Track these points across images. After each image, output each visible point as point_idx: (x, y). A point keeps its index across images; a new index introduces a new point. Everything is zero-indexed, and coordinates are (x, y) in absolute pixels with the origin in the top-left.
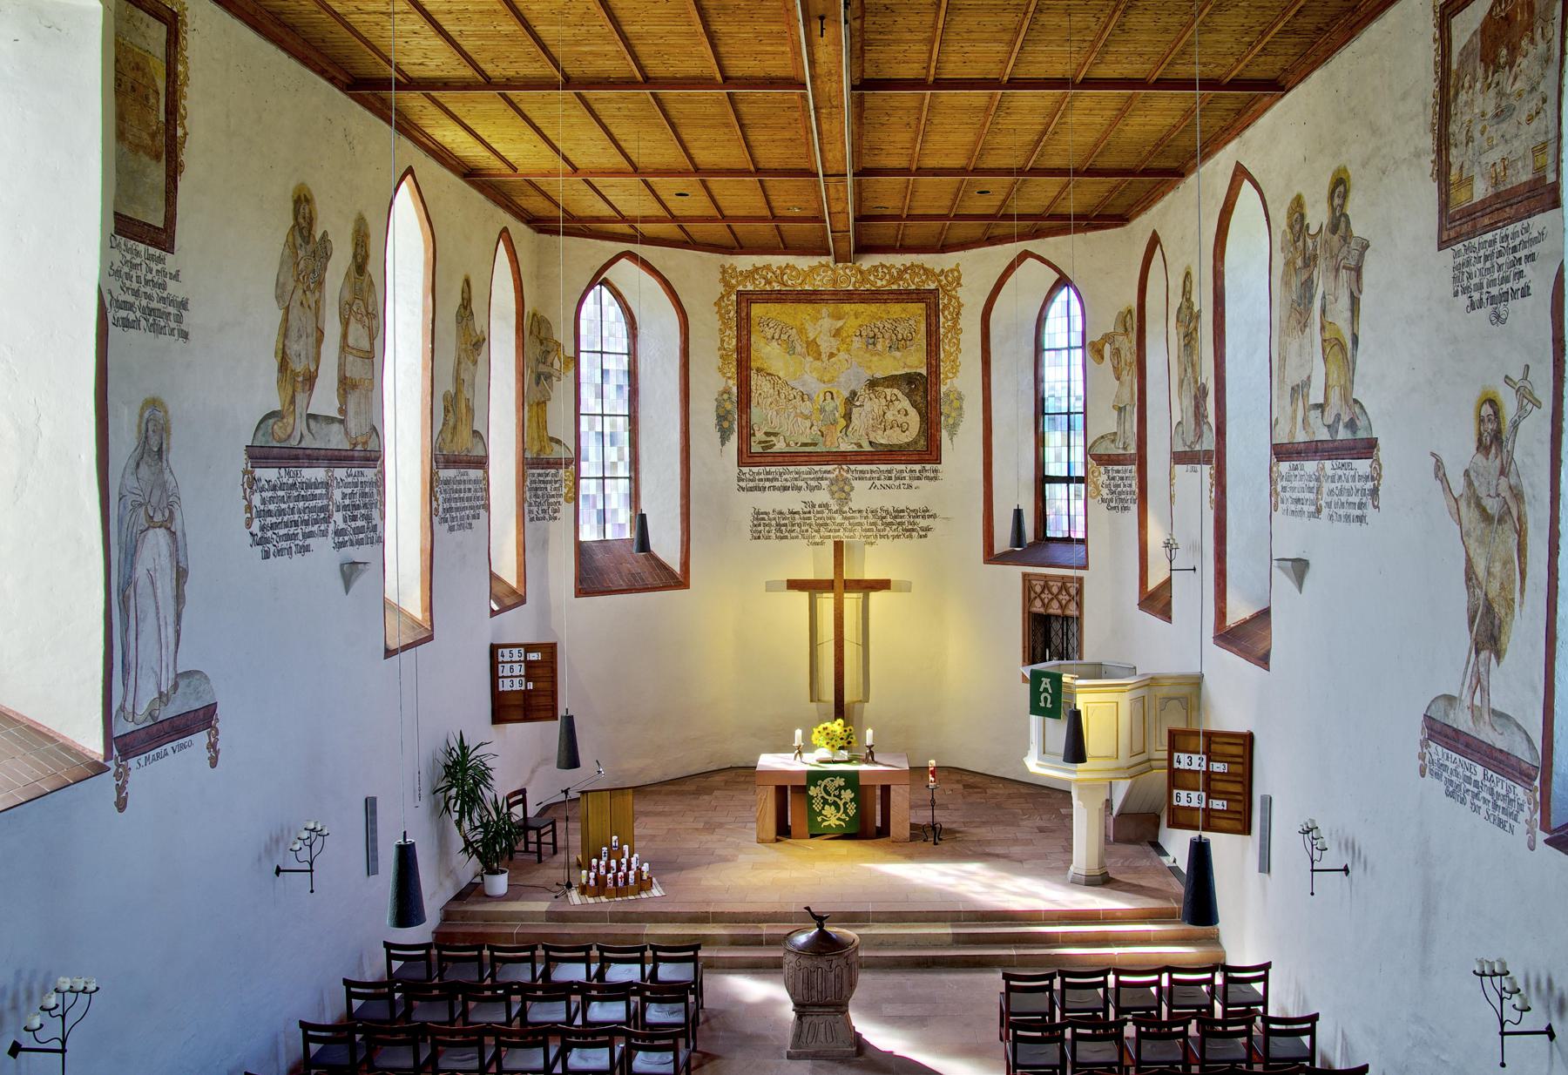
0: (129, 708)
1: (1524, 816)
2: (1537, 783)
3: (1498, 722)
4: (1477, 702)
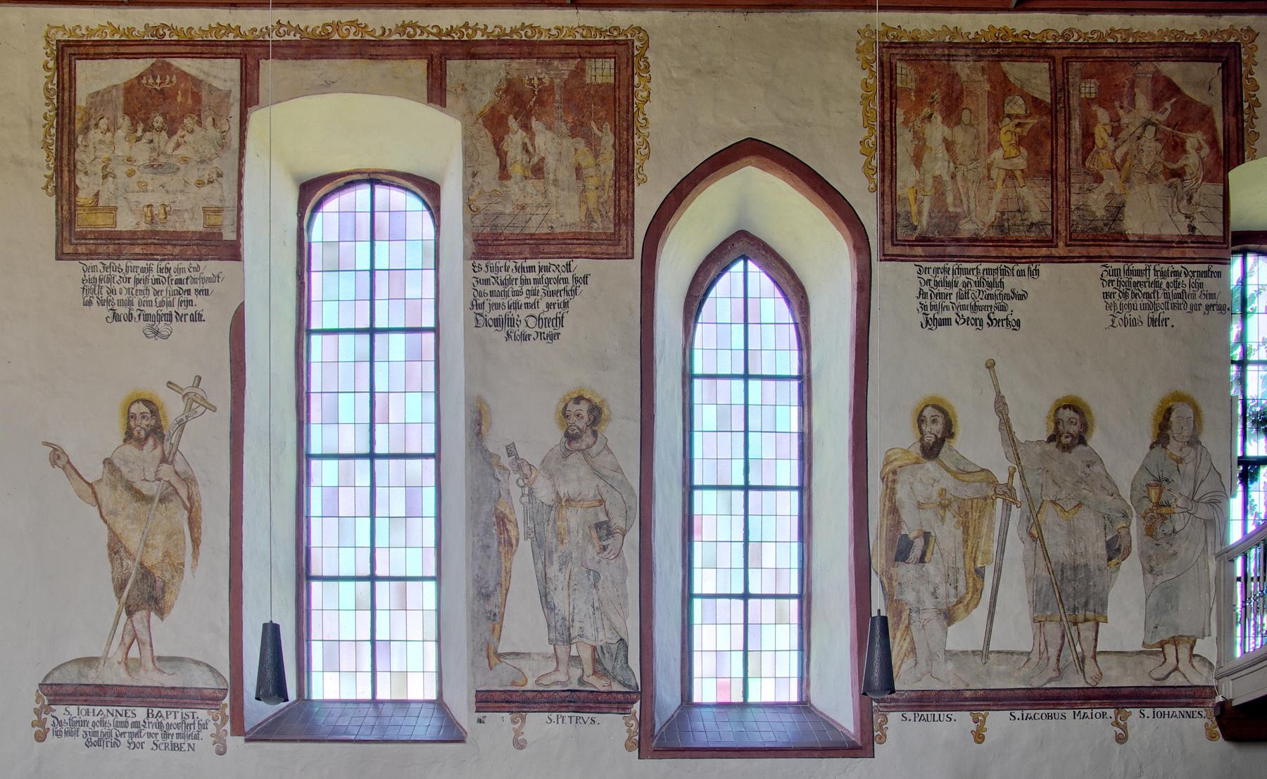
2: (227, 701)
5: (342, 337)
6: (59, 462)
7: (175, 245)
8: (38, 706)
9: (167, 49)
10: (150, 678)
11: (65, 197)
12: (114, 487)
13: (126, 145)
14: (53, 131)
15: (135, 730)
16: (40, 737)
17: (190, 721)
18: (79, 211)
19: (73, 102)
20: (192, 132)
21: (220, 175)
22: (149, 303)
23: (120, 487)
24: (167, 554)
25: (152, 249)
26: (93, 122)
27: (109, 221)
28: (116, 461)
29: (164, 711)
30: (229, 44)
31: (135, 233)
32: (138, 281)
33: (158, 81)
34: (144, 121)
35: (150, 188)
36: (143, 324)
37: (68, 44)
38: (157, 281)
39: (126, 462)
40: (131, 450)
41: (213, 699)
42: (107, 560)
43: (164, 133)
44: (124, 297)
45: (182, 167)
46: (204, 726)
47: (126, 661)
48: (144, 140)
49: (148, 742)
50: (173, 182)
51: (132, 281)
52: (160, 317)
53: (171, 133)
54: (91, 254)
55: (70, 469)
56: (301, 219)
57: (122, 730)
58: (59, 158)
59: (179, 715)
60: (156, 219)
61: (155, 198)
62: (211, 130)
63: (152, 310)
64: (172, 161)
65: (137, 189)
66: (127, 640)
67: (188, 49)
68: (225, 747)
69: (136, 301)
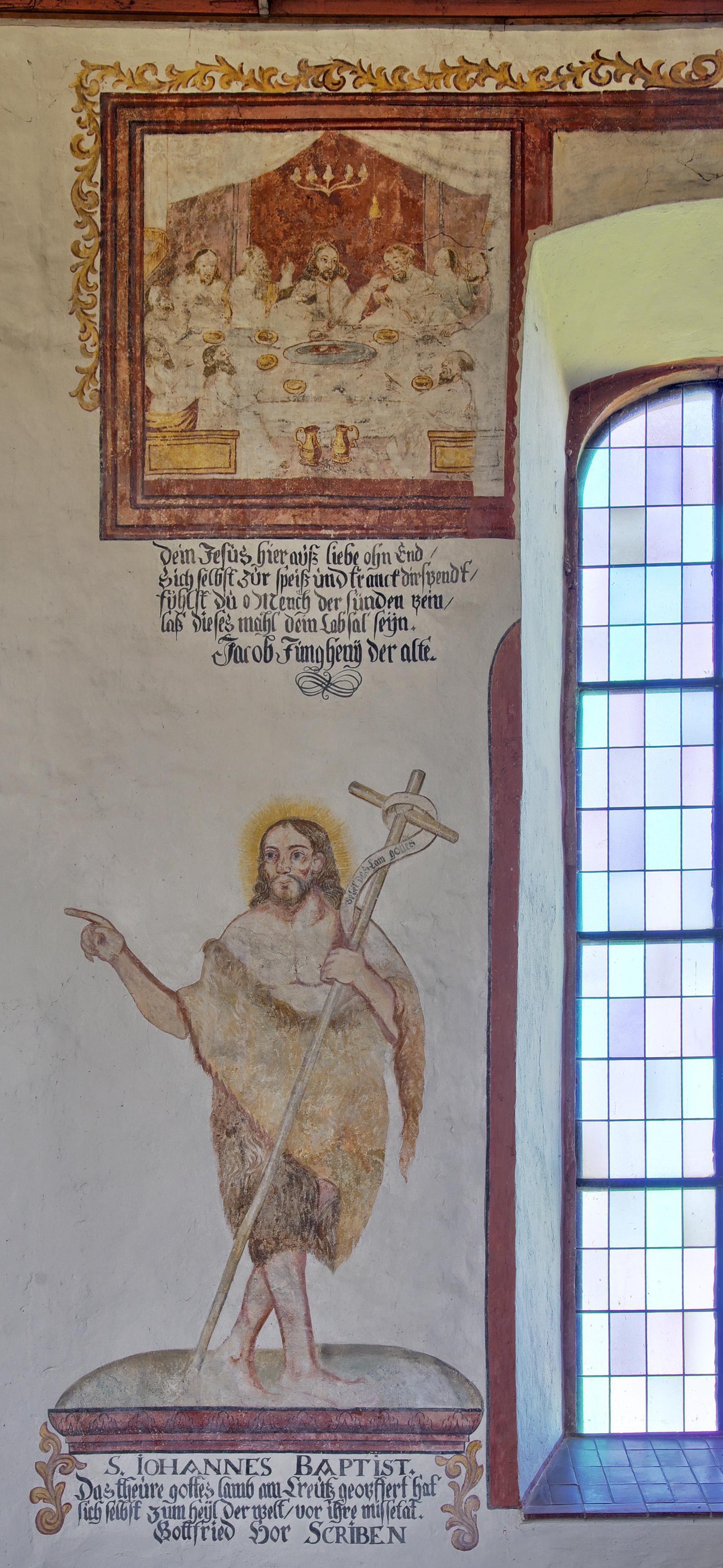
2: (480, 1434)
5: (653, 698)
6: (102, 950)
7: (366, 508)
8: (45, 1457)
9: (347, 112)
10: (306, 1390)
11: (121, 412)
12: (227, 998)
13: (259, 307)
14: (94, 279)
15: (269, 1502)
16: (49, 1525)
17: (395, 1478)
18: (154, 442)
19: (136, 219)
20: (403, 279)
21: (467, 366)
22: (310, 625)
23: (241, 998)
24: (344, 1133)
25: (316, 516)
26: (182, 260)
27: (222, 461)
28: (234, 946)
29: (334, 1460)
30: (485, 100)
31: (278, 483)
32: (283, 581)
33: (328, 176)
34: (296, 258)
35: (310, 392)
36: (295, 667)
37: (127, 101)
38: (327, 581)
39: (256, 949)
40: (267, 923)
41: (449, 1431)
42: (210, 1147)
43: (339, 283)
44: (254, 612)
45: (384, 350)
46: (428, 1489)
47: (250, 1357)
48: (296, 297)
49: (299, 1527)
50: (364, 381)
51: (272, 580)
52: (334, 654)
53: (356, 283)
54: (180, 526)
55: (129, 963)
56: (570, 460)
57: (237, 1502)
58: (108, 333)
59: (369, 1469)
60: (326, 455)
61: (325, 414)
62: (446, 278)
63: (317, 640)
64: (362, 337)
65: (282, 394)
66: (254, 1312)
67: (395, 112)
68: (474, 1533)
69: (279, 622)
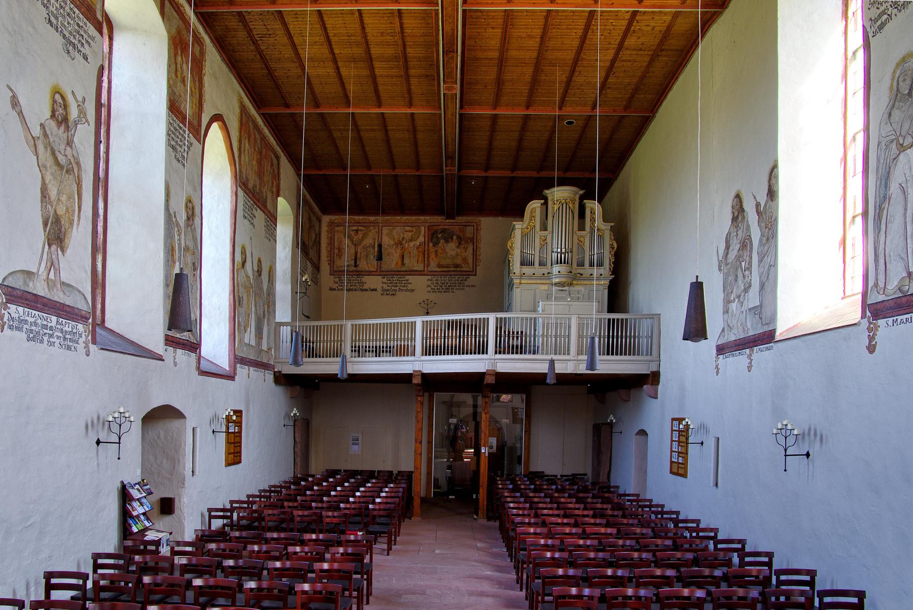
0: (881, 285)
1: (82, 340)
2: (90, 321)
3: (66, 289)
4: (52, 276)
